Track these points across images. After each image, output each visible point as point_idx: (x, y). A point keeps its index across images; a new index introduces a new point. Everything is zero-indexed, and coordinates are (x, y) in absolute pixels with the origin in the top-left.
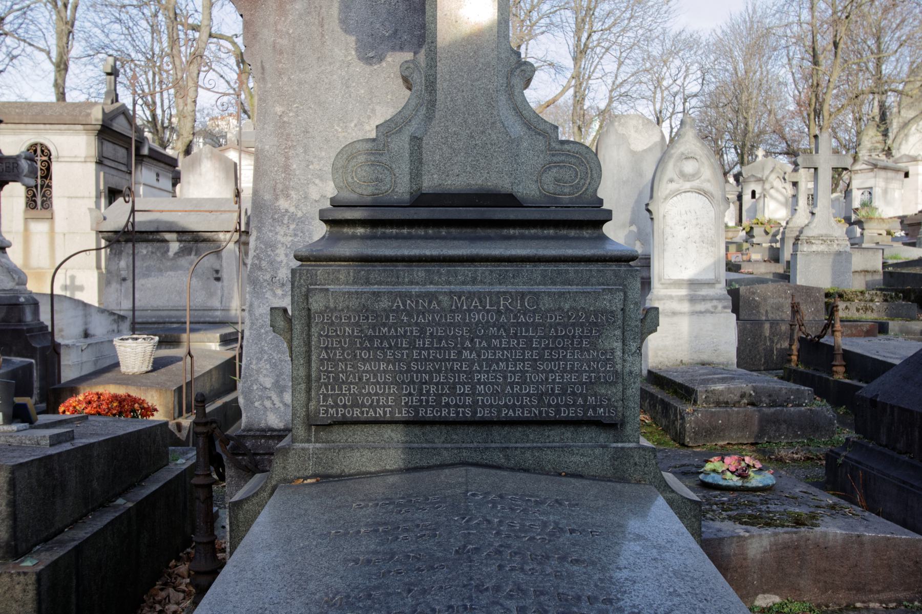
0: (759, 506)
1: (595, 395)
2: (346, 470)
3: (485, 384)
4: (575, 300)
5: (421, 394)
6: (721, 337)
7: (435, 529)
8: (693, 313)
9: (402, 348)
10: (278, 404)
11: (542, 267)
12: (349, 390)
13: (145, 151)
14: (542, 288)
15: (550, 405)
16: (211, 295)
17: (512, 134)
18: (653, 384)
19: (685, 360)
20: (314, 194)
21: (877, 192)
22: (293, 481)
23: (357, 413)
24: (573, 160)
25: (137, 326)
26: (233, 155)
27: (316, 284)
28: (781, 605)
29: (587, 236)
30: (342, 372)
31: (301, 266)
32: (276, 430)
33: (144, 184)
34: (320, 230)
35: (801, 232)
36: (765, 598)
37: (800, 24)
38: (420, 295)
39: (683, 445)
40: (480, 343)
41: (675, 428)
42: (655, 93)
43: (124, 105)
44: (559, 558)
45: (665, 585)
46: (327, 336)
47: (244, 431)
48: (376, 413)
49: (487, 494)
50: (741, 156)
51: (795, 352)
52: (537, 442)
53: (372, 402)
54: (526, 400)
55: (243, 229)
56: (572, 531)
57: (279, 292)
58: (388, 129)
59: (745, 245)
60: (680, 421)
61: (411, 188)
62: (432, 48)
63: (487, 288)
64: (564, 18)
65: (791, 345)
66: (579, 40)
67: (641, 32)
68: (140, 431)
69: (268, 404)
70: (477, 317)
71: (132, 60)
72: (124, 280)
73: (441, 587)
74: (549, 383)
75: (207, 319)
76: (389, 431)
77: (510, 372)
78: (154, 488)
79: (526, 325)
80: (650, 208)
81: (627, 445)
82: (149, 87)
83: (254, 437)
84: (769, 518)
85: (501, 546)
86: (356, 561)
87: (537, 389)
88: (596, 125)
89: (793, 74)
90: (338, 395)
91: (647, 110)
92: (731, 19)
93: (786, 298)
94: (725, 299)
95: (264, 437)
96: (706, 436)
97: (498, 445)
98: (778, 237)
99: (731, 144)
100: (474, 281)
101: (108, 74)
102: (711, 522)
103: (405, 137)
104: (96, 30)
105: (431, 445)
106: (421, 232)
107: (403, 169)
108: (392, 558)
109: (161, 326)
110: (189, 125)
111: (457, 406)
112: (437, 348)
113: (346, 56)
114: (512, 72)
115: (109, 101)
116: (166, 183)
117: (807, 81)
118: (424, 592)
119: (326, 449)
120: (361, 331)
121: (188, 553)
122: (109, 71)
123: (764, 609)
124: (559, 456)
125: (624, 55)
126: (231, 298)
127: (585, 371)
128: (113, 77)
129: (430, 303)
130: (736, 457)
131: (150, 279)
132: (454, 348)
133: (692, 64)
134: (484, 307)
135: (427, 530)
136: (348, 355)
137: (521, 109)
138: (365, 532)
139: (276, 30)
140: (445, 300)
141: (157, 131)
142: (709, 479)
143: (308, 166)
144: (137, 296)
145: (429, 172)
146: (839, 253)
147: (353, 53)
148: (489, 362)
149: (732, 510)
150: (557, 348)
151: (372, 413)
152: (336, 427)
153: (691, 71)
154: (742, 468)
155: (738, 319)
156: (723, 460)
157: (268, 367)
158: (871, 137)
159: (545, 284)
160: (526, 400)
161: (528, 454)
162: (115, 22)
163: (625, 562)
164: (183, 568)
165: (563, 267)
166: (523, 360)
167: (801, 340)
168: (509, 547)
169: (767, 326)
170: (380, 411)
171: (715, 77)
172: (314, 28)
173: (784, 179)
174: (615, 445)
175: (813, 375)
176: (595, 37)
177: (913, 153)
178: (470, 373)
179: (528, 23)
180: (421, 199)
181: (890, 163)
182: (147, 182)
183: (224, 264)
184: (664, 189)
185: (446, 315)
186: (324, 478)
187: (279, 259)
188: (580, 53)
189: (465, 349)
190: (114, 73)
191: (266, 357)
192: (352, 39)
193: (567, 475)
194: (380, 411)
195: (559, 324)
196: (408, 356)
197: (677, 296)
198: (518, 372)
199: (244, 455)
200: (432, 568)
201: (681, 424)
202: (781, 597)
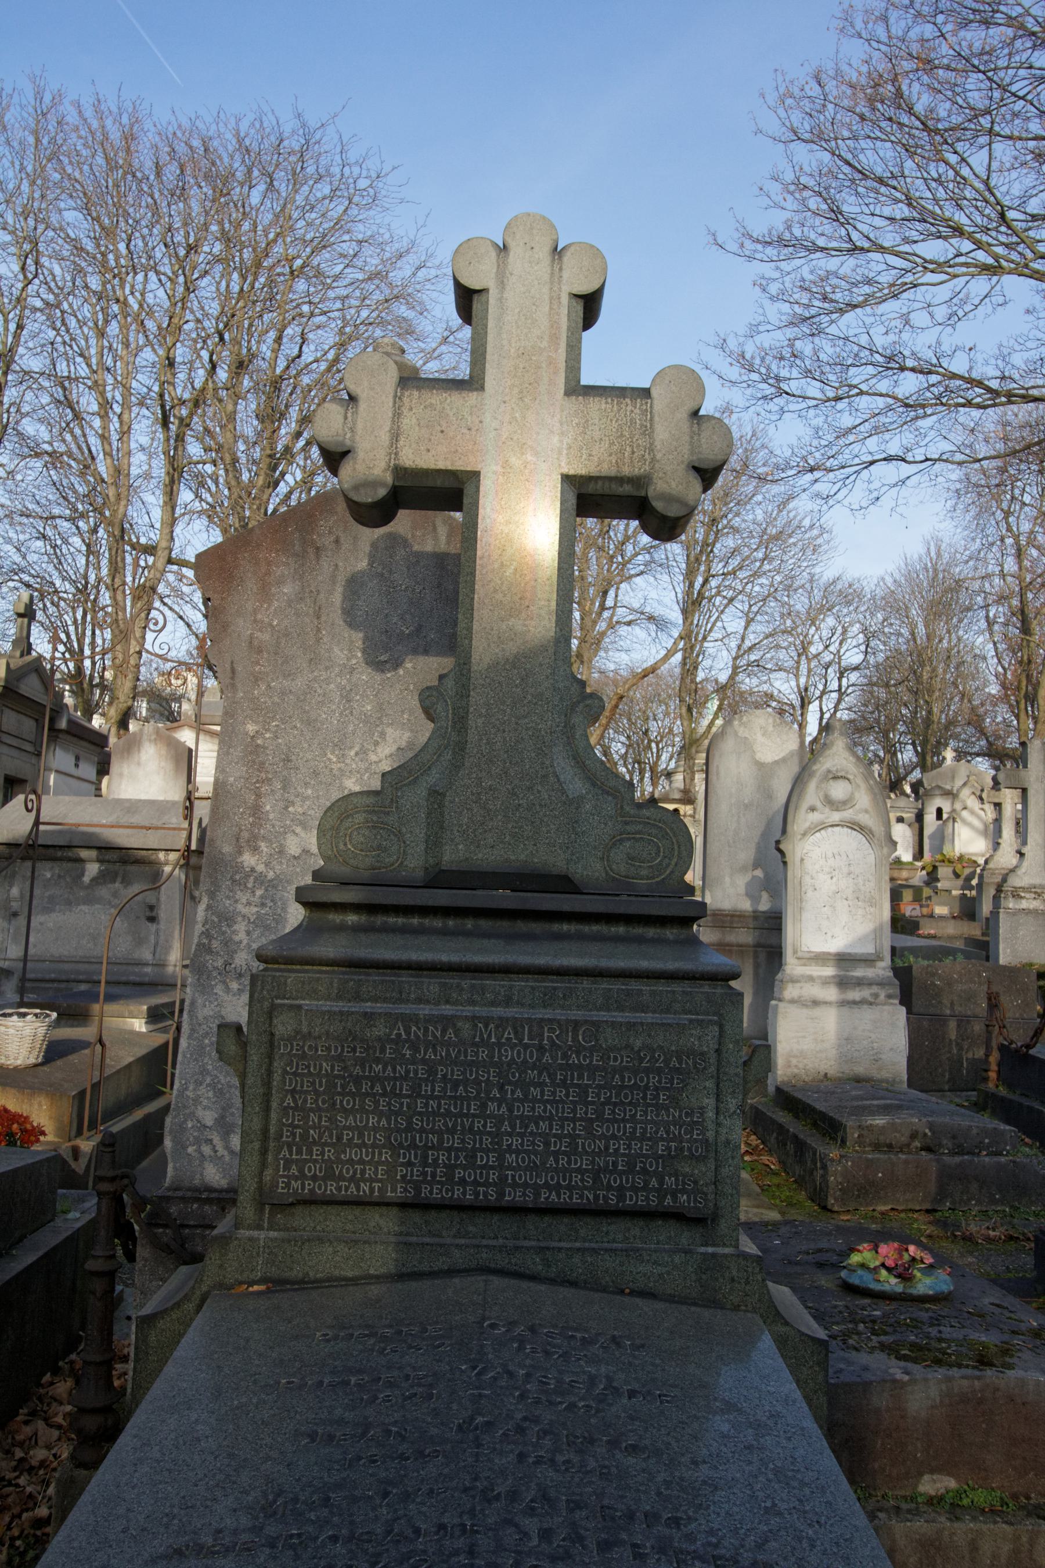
0: (927, 1329)
1: (676, 1175)
2: (311, 1274)
3: (518, 1152)
4: (649, 1036)
5: (425, 1164)
6: (886, 1037)
7: (431, 1386)
8: (843, 1003)
9: (400, 1096)
10: (221, 1151)
11: (604, 985)
12: (323, 1154)
13: (63, 724)
14: (603, 1016)
15: (609, 1187)
16: (140, 942)
17: (570, 793)
18: (783, 1109)
19: (832, 1072)
20: (293, 847)
22: (231, 1287)
23: (331, 1188)
24: (654, 831)
25: (28, 985)
26: (187, 736)
27: (284, 998)
28: (959, 1494)
29: (671, 937)
30: (314, 1127)
31: (265, 970)
32: (215, 1190)
33: (57, 771)
34: (296, 914)
35: (1004, 880)
36: (934, 1481)
37: (1003, 575)
38: (430, 1019)
39: (825, 1208)
40: (513, 1092)
41: (814, 1181)
42: (798, 662)
43: (40, 657)
44: (608, 1442)
45: (761, 1494)
46: (295, 1074)
47: (169, 1189)
48: (358, 1190)
49: (512, 1324)
50: (922, 756)
51: (994, 1067)
52: (590, 1241)
53: (355, 1173)
54: (576, 1178)
55: (193, 847)
56: (632, 1394)
57: (234, 986)
58: (397, 780)
59: (927, 892)
60: (821, 1172)
61: (427, 861)
62: (465, 672)
63: (526, 1013)
64: (670, 555)
65: (987, 1056)
66: (691, 585)
67: (778, 578)
68: (15, 1171)
69: (206, 1150)
70: (509, 1054)
71: (56, 592)
72: (15, 915)
73: (431, 1491)
74: (610, 1155)
75: (132, 978)
76: (377, 1217)
77: (555, 1136)
78: (31, 1259)
79: (580, 1067)
80: (782, 847)
81: (720, 1250)
82: (77, 629)
83: (183, 1199)
84: (939, 1350)
85: (525, 1419)
86: (312, 1436)
87: (593, 1162)
88: (713, 705)
89: (995, 644)
90: (306, 1161)
91: (786, 685)
92: (906, 565)
93: (980, 984)
94: (890, 984)
95: (197, 1200)
96: (859, 1196)
97: (533, 1243)
98: (974, 882)
99: (908, 739)
100: (508, 1002)
101: (20, 615)
102: (854, 1353)
103: (422, 791)
104: (9, 547)
105: (437, 1240)
106: (438, 923)
107: (416, 833)
108: (364, 1434)
109: (63, 985)
110: (128, 684)
111: (476, 1183)
112: (450, 1097)
113: (348, 659)
114: (573, 707)
115: (18, 654)
116: (88, 770)
117: (1014, 653)
118: (406, 1497)
119: (283, 1241)
120: (345, 1069)
121: (72, 1362)
122: (22, 610)
123: (931, 1498)
124: (622, 1264)
125: (755, 609)
126: (168, 949)
127: (662, 1139)
128: (26, 620)
129: (444, 1031)
130: (896, 1245)
131: (53, 915)
132: (475, 1098)
133: (851, 625)
134: (521, 1040)
135: (419, 1385)
136: (324, 1103)
137: (582, 759)
138: (330, 1385)
139: (255, 621)
140: (466, 1027)
141: (83, 690)
142: (854, 1280)
143: (287, 807)
144: (31, 939)
145: (452, 840)
147: (359, 655)
148: (525, 1121)
149: (886, 1333)
150: (622, 1103)
151: (353, 1189)
152: (300, 1209)
153: (850, 635)
154: (903, 1265)
156: (876, 1249)
157: (211, 1094)
159: (608, 1010)
160: (576, 1178)
161: (576, 1259)
162: (38, 538)
163: (705, 1451)
164: (63, 1387)
165: (634, 985)
166: (574, 1120)
167: (1002, 1048)
168: (536, 1421)
169: (952, 1024)
170: (365, 1187)
171: (885, 644)
172: (307, 620)
173: (981, 798)
174: (702, 1249)
175: (1020, 1104)
176: (714, 583)
178: (497, 1135)
179: (620, 559)
180: (439, 878)
182: (62, 768)
183: (163, 898)
184: (802, 820)
185: (466, 1051)
186: (278, 1284)
187: (237, 938)
188: (692, 604)
189: (492, 1100)
190: (28, 614)
191: (208, 1080)
192: (358, 637)
193: (632, 1293)
194: (365, 1187)
195: (627, 1068)
196: (408, 1107)
197: (820, 977)
198: (565, 1136)
199: (165, 1226)
200: (421, 1454)
201: (822, 1176)
202: (958, 1481)
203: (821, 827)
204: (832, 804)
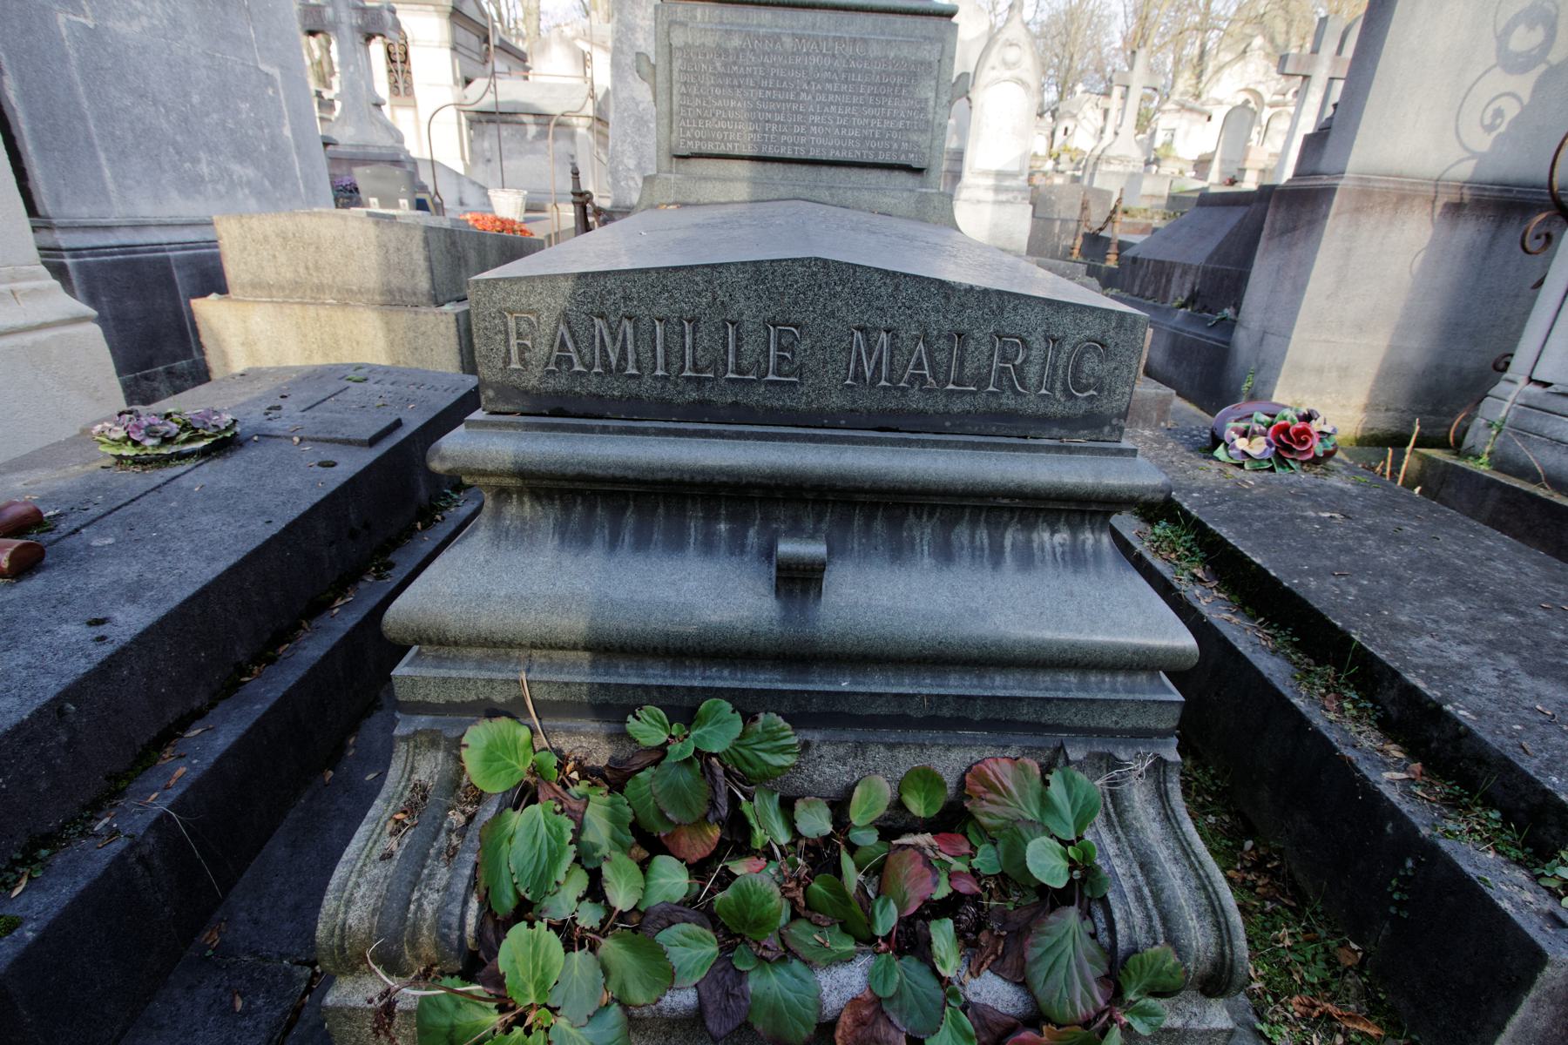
6: (1019, 223)
21: (1179, 135)
54: (851, 142)
69: (632, 183)
70: (815, 60)
146: (1133, 175)
155: (1034, 215)
158: (1185, 81)
160: (851, 142)
169: (1058, 223)
177: (1220, 97)
181: (1197, 105)
203: (997, 81)
204: (1007, 65)
